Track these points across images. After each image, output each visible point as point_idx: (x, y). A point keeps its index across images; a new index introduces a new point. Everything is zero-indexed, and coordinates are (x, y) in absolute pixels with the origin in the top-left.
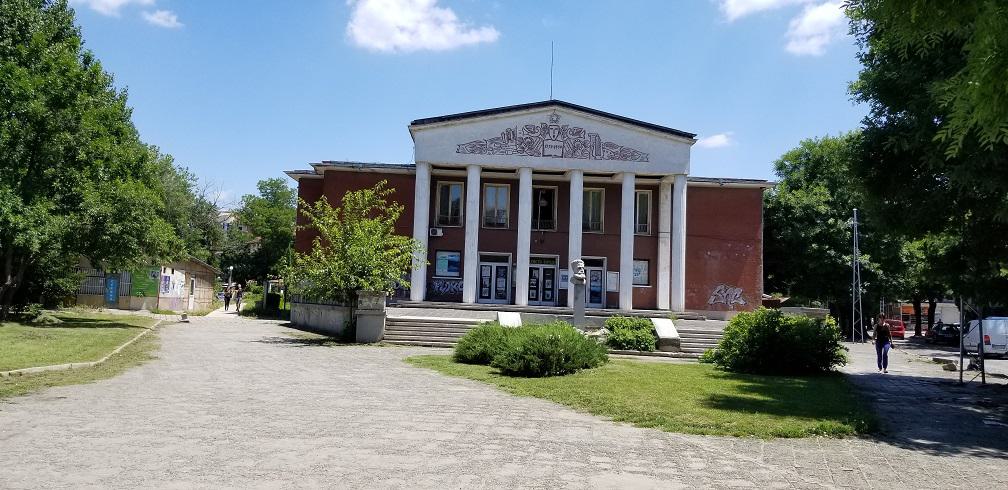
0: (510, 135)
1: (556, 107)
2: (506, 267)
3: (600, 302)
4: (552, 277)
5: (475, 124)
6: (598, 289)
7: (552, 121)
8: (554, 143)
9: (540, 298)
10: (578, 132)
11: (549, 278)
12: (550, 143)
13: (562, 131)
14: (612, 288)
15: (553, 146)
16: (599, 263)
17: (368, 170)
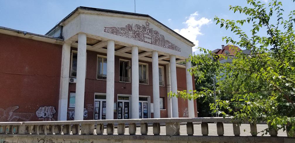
0: (129, 27)
2: (125, 103)
5: (113, 18)
8: (148, 36)
10: (157, 33)
11: (126, 107)
13: (151, 31)
14: (152, 111)
15: (148, 37)
16: (146, 99)
17: (27, 36)
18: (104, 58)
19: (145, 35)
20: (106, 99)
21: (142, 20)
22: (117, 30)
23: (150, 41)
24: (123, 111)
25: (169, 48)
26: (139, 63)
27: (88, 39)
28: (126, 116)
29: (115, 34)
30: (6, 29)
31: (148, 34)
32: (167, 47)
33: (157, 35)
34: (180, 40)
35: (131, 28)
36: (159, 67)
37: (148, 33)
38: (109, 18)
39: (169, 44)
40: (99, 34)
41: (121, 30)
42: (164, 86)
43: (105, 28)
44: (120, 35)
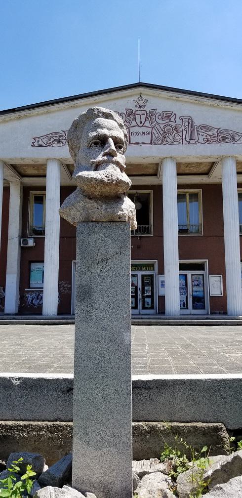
1: (141, 89)
2: (143, 276)
3: (203, 308)
4: (151, 284)
5: (52, 115)
6: (200, 294)
7: (138, 106)
9: (140, 306)
10: (168, 116)
11: (148, 284)
12: (137, 129)
13: (150, 116)
16: (200, 267)
21: (124, 99)
22: (62, 136)
23: (147, 139)
24: (139, 293)
25: (208, 141)
26: (239, 189)
27: (179, 165)
28: (148, 303)
29: (54, 145)
32: (201, 140)
33: (168, 121)
34: (19, 118)
36: (238, 191)
37: (141, 122)
38: (44, 117)
39: (210, 133)
40: (27, 154)
43: (34, 139)
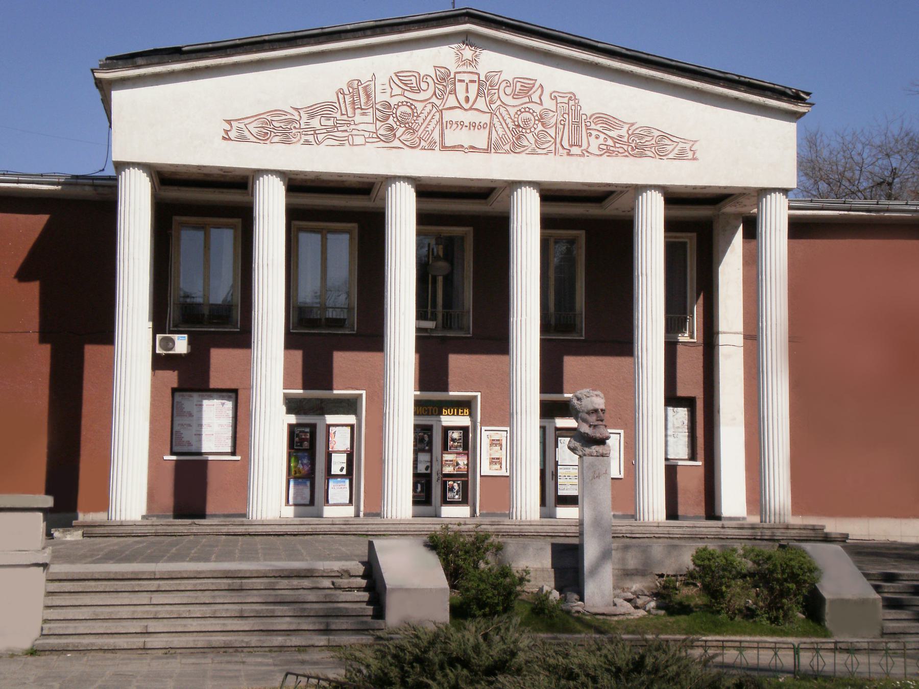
18: (43, 624)
19: (448, 116)
20: (285, 394)
22: (292, 121)
23: (480, 139)
25: (608, 152)
30: (335, 616)
31: (467, 106)
32: (594, 149)
33: (527, 100)
35: (368, 96)
41: (312, 116)
42: (583, 338)
43: (229, 122)
44: (307, 142)
